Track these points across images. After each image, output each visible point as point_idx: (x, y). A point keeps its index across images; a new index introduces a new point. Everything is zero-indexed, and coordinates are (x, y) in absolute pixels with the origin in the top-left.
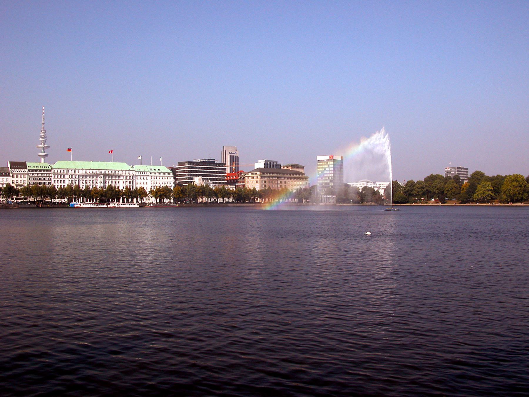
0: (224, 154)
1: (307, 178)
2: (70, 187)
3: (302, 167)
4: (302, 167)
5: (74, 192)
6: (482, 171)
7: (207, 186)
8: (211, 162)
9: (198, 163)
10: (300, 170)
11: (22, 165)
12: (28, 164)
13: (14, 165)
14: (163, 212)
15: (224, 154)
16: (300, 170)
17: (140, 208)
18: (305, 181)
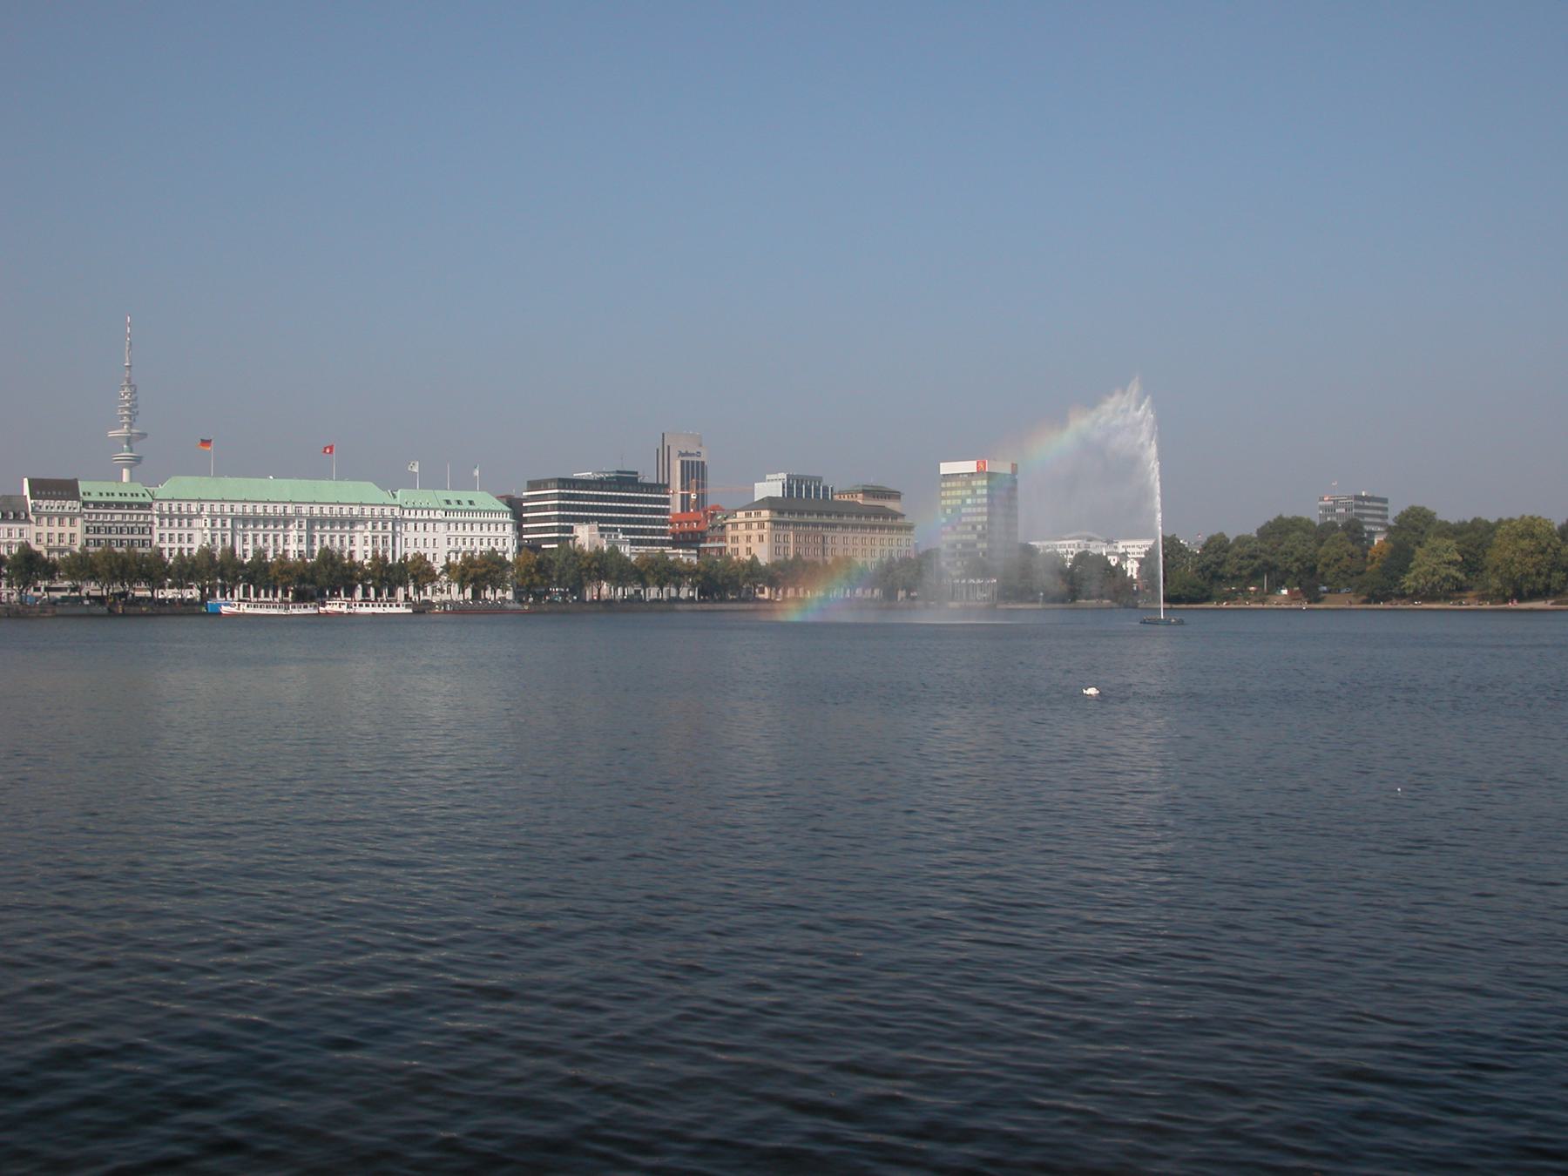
1: (909, 528)
2: (207, 553)
3: (895, 495)
4: (895, 495)
7: (614, 550)
8: (626, 481)
10: (891, 505)
12: (83, 486)
13: (42, 488)
15: (663, 455)
16: (891, 505)
18: (903, 537)
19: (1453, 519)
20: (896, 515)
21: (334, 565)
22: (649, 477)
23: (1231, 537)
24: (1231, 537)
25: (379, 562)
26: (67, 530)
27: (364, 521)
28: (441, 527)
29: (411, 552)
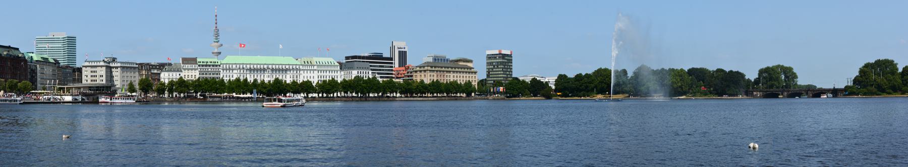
0: (392, 48)
1: (475, 73)
2: (238, 80)
3: (471, 61)
4: (471, 61)
5: (241, 86)
6: (698, 66)
7: (374, 78)
8: (378, 57)
9: (363, 58)
10: (469, 65)
11: (193, 61)
12: (198, 60)
13: (186, 61)
14: (900, 100)
15: (392, 48)
16: (469, 65)
17: (136, 110)
18: (474, 75)
19: (843, 87)
20: (471, 68)
21: (681, 76)
22: (386, 54)
23: (747, 77)
24: (747, 77)
25: (294, 83)
26: (312, 75)
27: (290, 70)
28: (316, 72)
29: (305, 80)
